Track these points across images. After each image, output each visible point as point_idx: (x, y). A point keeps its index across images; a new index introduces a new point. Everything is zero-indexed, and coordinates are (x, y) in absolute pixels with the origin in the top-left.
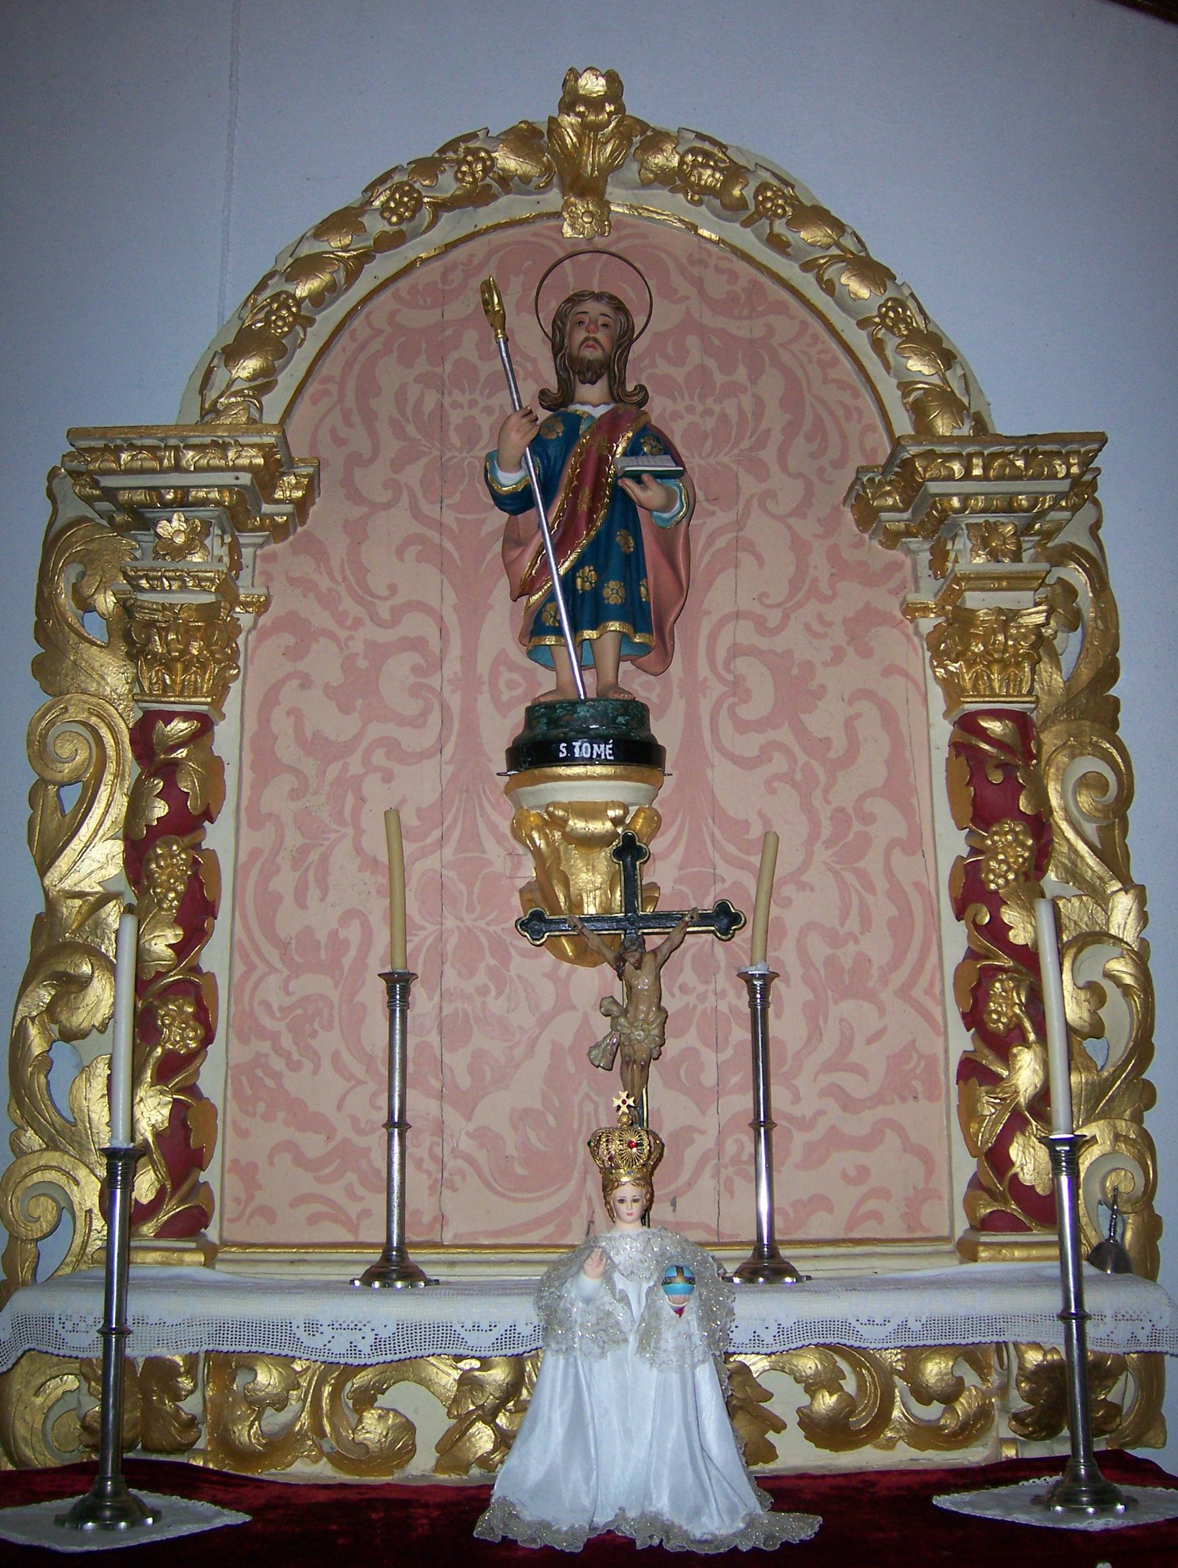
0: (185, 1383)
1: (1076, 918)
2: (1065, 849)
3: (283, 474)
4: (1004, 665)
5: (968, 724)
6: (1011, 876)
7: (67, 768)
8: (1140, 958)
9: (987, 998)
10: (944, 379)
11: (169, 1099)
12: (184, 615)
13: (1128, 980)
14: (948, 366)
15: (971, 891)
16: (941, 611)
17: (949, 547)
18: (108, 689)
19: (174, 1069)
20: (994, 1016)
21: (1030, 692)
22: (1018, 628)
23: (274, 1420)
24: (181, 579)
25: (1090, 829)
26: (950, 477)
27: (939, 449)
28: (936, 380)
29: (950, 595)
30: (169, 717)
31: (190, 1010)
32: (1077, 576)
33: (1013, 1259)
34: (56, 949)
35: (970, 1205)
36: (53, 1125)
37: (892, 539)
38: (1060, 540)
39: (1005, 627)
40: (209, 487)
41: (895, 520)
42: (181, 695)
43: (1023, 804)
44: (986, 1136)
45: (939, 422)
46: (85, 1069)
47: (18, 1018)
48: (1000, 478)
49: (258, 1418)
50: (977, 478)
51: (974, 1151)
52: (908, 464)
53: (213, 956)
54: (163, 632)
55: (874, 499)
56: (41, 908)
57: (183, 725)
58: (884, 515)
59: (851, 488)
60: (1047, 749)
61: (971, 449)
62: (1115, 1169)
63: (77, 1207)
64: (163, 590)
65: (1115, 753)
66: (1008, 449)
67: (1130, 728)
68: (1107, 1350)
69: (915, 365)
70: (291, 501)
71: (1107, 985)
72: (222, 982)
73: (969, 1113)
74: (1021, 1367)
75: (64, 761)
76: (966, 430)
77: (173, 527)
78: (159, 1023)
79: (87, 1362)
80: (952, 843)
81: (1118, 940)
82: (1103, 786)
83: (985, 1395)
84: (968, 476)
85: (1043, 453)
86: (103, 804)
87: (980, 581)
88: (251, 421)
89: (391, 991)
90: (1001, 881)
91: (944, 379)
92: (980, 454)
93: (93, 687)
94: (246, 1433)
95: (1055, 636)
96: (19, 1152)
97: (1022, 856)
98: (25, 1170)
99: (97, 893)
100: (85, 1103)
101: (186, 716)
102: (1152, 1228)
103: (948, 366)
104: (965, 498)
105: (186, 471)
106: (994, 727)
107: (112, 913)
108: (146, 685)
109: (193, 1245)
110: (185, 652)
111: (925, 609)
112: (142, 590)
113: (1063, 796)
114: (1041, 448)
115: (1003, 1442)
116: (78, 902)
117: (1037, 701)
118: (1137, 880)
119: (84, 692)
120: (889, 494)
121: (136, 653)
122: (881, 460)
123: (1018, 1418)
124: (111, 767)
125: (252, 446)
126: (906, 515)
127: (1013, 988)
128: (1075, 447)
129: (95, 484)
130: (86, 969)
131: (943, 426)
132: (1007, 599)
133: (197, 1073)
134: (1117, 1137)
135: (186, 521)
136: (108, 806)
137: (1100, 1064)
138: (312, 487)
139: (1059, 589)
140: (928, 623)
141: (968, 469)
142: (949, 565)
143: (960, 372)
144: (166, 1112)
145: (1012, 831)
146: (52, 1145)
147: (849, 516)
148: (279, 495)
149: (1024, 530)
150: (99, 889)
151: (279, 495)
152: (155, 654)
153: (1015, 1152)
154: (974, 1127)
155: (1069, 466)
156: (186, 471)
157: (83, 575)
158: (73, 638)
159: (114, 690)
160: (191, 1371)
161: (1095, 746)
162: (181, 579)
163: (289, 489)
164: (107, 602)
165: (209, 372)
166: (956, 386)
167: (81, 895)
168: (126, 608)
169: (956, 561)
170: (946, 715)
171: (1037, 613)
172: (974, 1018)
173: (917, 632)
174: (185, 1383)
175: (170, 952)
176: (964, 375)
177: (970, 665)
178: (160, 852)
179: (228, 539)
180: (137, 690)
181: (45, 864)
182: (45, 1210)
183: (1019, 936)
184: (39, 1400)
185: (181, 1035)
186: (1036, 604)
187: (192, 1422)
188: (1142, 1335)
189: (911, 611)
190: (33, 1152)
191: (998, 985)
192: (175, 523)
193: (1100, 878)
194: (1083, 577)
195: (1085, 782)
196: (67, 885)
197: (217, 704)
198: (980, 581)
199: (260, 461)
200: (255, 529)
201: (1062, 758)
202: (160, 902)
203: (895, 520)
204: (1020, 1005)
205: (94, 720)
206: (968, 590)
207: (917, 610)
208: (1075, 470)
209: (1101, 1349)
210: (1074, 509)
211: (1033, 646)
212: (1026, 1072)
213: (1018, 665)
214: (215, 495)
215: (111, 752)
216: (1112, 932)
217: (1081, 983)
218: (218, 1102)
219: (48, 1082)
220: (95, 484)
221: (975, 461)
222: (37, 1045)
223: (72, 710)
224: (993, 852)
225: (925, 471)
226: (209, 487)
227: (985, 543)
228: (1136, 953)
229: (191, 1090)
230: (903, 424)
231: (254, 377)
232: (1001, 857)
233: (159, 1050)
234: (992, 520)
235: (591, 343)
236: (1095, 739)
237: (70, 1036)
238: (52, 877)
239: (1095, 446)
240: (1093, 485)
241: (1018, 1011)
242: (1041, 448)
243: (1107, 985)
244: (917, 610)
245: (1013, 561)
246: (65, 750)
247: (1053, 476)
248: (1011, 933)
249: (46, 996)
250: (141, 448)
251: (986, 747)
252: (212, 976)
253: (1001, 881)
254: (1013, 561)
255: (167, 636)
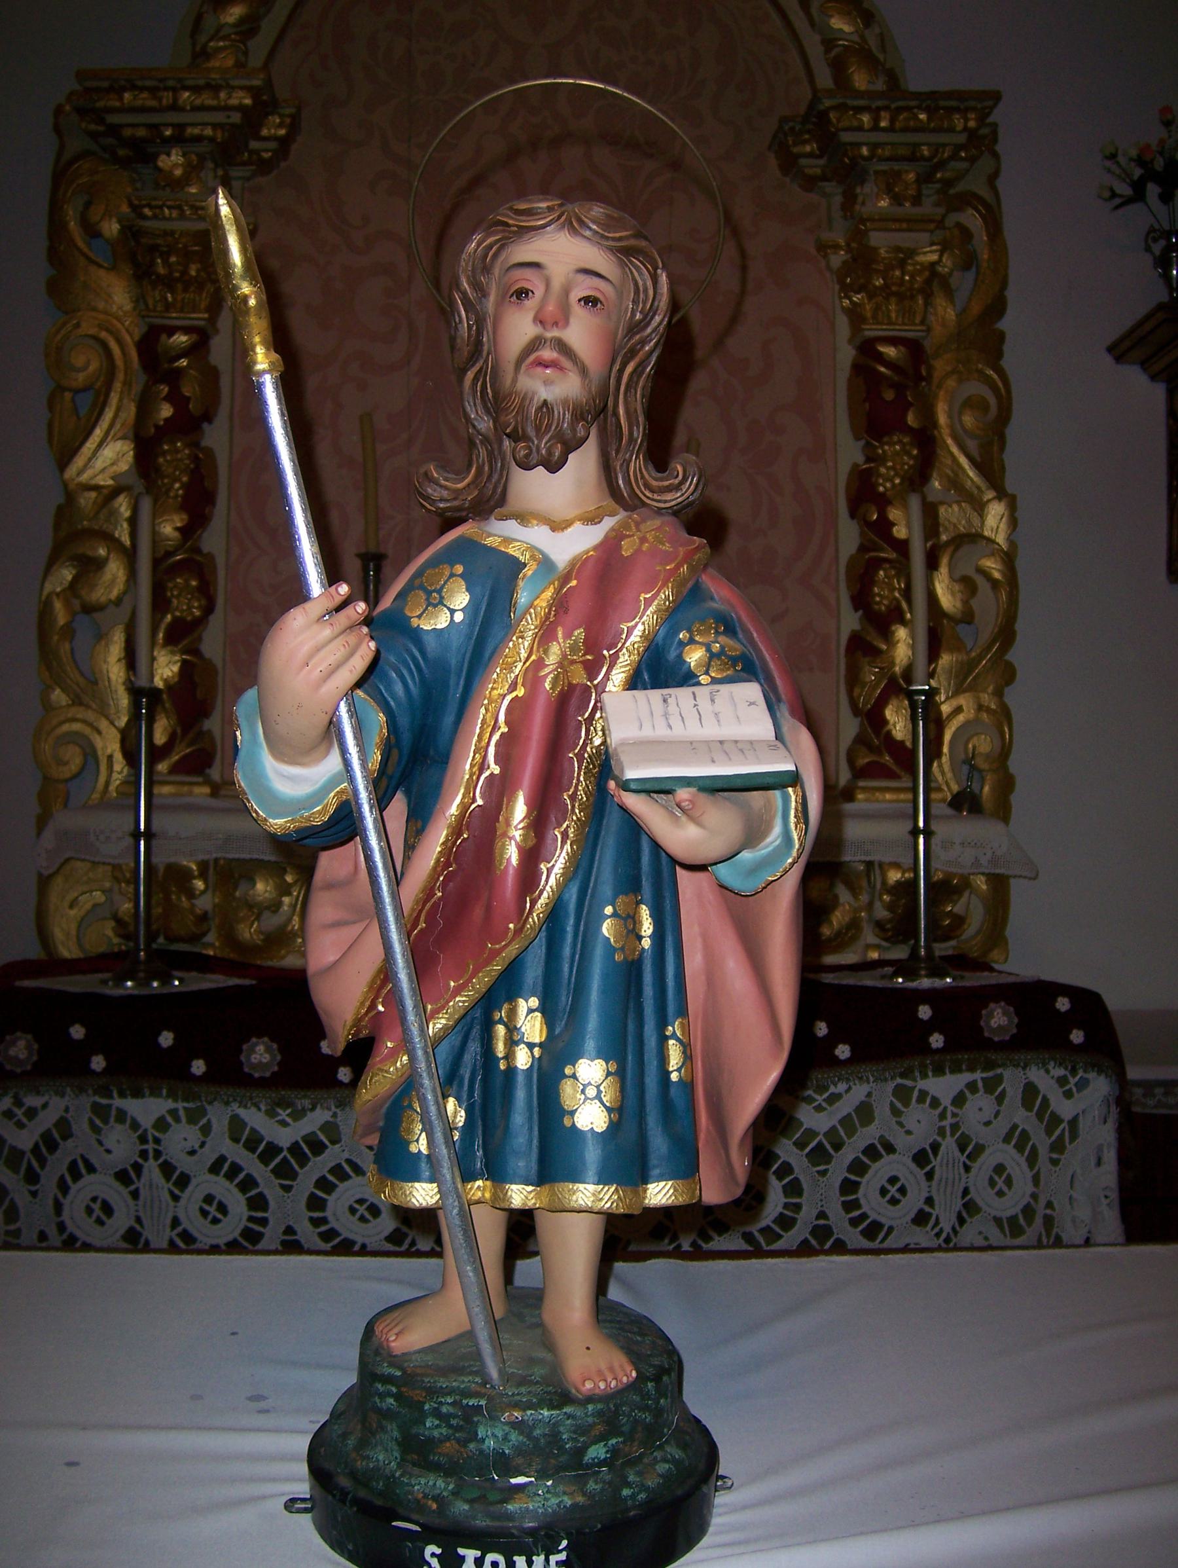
0: (199, 884)
1: (955, 521)
2: (949, 462)
3: (267, 114)
4: (901, 297)
5: (867, 349)
6: (897, 481)
7: (81, 377)
8: (1009, 559)
9: (872, 583)
10: (862, 37)
11: (177, 658)
12: (184, 240)
13: (997, 575)
14: (867, 25)
15: (864, 493)
16: (849, 249)
17: (858, 190)
18: (115, 308)
19: (181, 634)
20: (878, 599)
21: (922, 322)
22: (914, 265)
23: (271, 922)
24: (180, 208)
25: (972, 445)
26: (860, 129)
27: (851, 102)
28: (856, 38)
29: (858, 235)
30: (172, 331)
31: (194, 583)
32: (972, 219)
33: (885, 801)
34: (74, 535)
35: (851, 761)
36: (78, 684)
37: (810, 183)
38: (960, 187)
39: (902, 264)
40: (203, 127)
41: (814, 166)
42: (182, 311)
43: (911, 419)
44: (866, 700)
45: (856, 77)
46: (101, 636)
47: (45, 593)
48: (905, 130)
49: (258, 918)
50: (884, 130)
51: (856, 711)
52: (823, 116)
53: (213, 541)
54: (165, 256)
55: (795, 144)
56: (61, 500)
57: (184, 338)
58: (803, 161)
59: (775, 137)
60: (937, 375)
61: (880, 103)
62: (977, 734)
63: (100, 753)
64: (165, 218)
65: (995, 376)
66: (913, 103)
67: (1016, 359)
68: (954, 870)
69: (839, 24)
70: (276, 138)
71: (980, 581)
72: (220, 561)
73: (853, 678)
74: (884, 882)
75: (79, 370)
76: (880, 85)
77: (173, 161)
78: (169, 594)
79: (116, 867)
80: (849, 453)
81: (989, 540)
82: (986, 408)
83: (857, 910)
84: (876, 128)
85: (943, 108)
86: (113, 408)
87: (884, 221)
88: (240, 65)
89: (366, 570)
90: (888, 485)
91: (862, 37)
92: (886, 108)
93: (101, 305)
94: (249, 932)
95: (950, 274)
96: (48, 707)
97: (907, 464)
98: (55, 722)
99: (109, 486)
100: (105, 667)
101: (186, 330)
102: (1006, 784)
103: (867, 25)
104: (874, 147)
105: (182, 110)
106: (890, 351)
107: (123, 506)
108: (151, 303)
109: (200, 779)
110: (185, 272)
111: (836, 247)
112: (145, 218)
113: (950, 417)
114: (942, 103)
115: (869, 947)
116: (93, 494)
117: (929, 330)
118: (1010, 491)
119: (94, 309)
120: (805, 142)
121: (142, 275)
122: (802, 109)
123: (879, 925)
124: (120, 376)
125: (242, 88)
126: (822, 162)
127: (894, 576)
128: (972, 103)
129: (102, 121)
130: (102, 552)
131: (860, 80)
132: (905, 239)
133: (200, 639)
134: (980, 708)
135: (184, 155)
136: (118, 410)
137: (969, 647)
138: (294, 127)
139: (956, 232)
140: (838, 259)
141: (876, 120)
142: (857, 207)
143: (877, 30)
144: (176, 668)
145: (900, 442)
146: (77, 701)
147: (772, 162)
148: (265, 132)
149: (925, 178)
150: (111, 482)
151: (265, 132)
152: (158, 276)
153: (889, 713)
154: (857, 691)
155: (966, 120)
156: (182, 110)
157: (88, 205)
158: (82, 262)
159: (120, 308)
160: (203, 875)
161: (981, 372)
162: (180, 208)
163: (274, 128)
164: (112, 228)
165: (199, 18)
166: (873, 43)
167: (97, 488)
168: (131, 232)
169: (863, 203)
170: (850, 341)
171: (931, 252)
172: (861, 599)
173: (828, 267)
174: (199, 884)
175: (176, 534)
176: (881, 34)
177: (871, 297)
178: (166, 447)
179: (220, 172)
180: (142, 307)
181: (63, 462)
182: (74, 758)
183: (900, 532)
184: (72, 912)
185: (188, 604)
186: (932, 244)
187: (204, 917)
188: (984, 861)
189: (823, 248)
190: (61, 707)
191: (881, 573)
192: (173, 158)
193: (978, 488)
194: (979, 221)
195: (970, 403)
196: (84, 478)
197: (213, 320)
198: (884, 221)
199: (248, 101)
200: (244, 164)
201: (951, 383)
202: (168, 490)
203: (814, 166)
204: (900, 590)
205: (103, 334)
206: (875, 230)
207: (830, 247)
208: (972, 124)
209: (950, 870)
210: (972, 160)
211: (928, 282)
212: (904, 646)
213: (912, 297)
214: (208, 132)
215: (119, 363)
216: (986, 534)
217: (957, 575)
218: (218, 662)
219: (72, 650)
220: (102, 121)
221: (883, 114)
222: (61, 618)
223: (84, 325)
224: (882, 460)
225: (839, 120)
226: (203, 127)
227: (889, 190)
228: (1006, 553)
229: (195, 651)
230: (825, 80)
231: (242, 21)
232: (890, 464)
233: (169, 617)
234: (896, 168)
235: (547, 354)
236: (980, 366)
237: (89, 609)
238: (71, 472)
239: (990, 103)
240: (994, 136)
241: (897, 595)
242: (942, 103)
243: (980, 581)
244: (830, 247)
245: (913, 204)
246: (79, 360)
247: (951, 130)
248: (895, 529)
249: (67, 574)
250: (142, 89)
251: (883, 369)
252: (211, 557)
253: (888, 485)
254: (913, 204)
255: (168, 259)
